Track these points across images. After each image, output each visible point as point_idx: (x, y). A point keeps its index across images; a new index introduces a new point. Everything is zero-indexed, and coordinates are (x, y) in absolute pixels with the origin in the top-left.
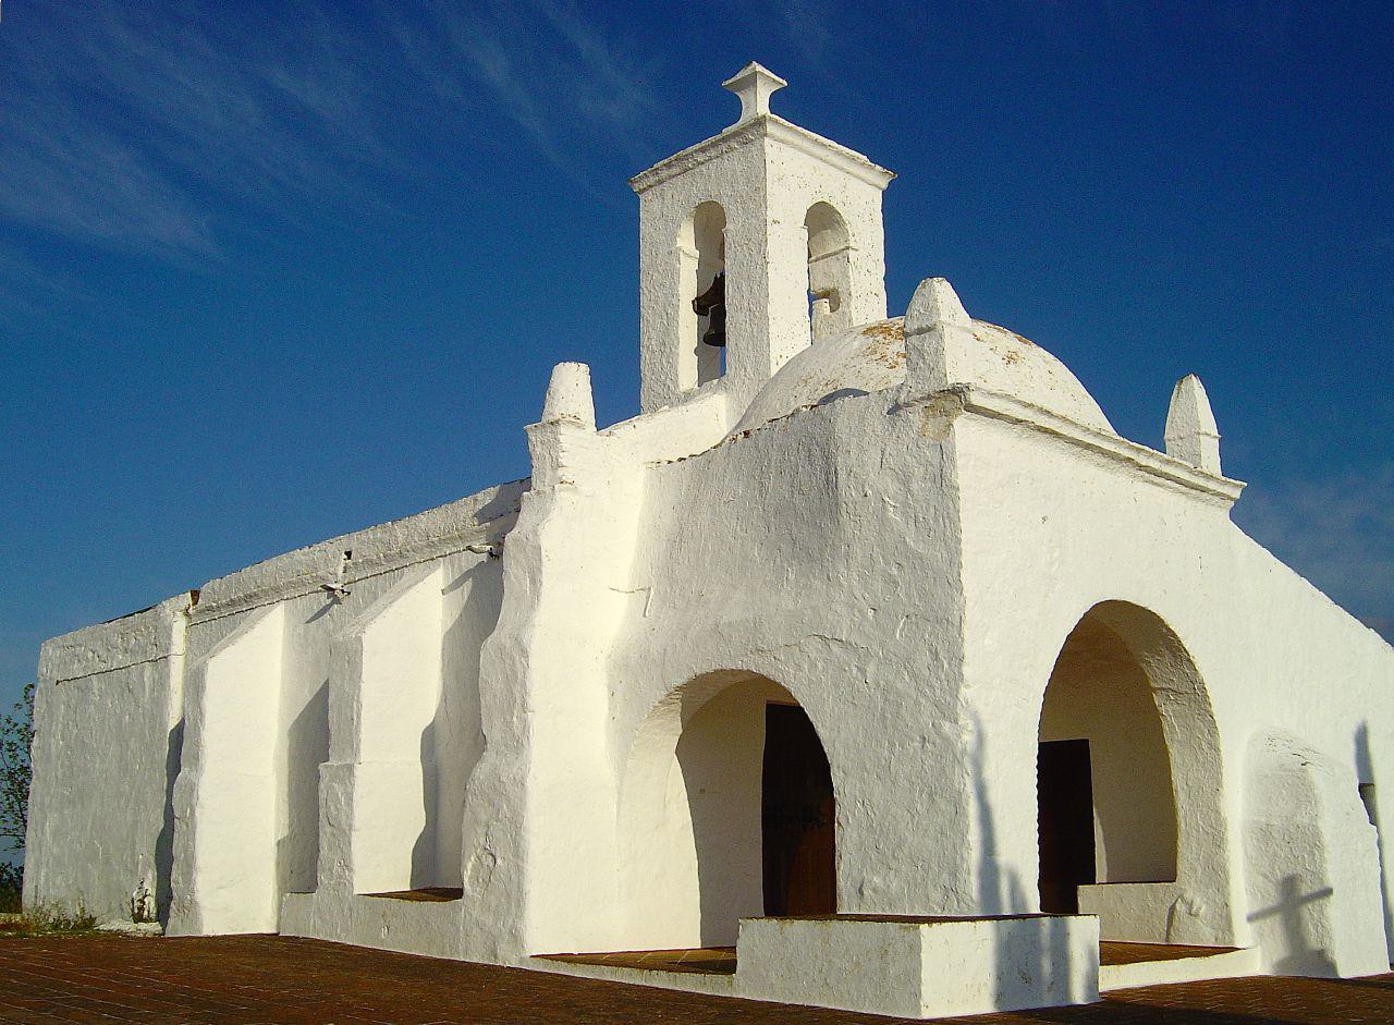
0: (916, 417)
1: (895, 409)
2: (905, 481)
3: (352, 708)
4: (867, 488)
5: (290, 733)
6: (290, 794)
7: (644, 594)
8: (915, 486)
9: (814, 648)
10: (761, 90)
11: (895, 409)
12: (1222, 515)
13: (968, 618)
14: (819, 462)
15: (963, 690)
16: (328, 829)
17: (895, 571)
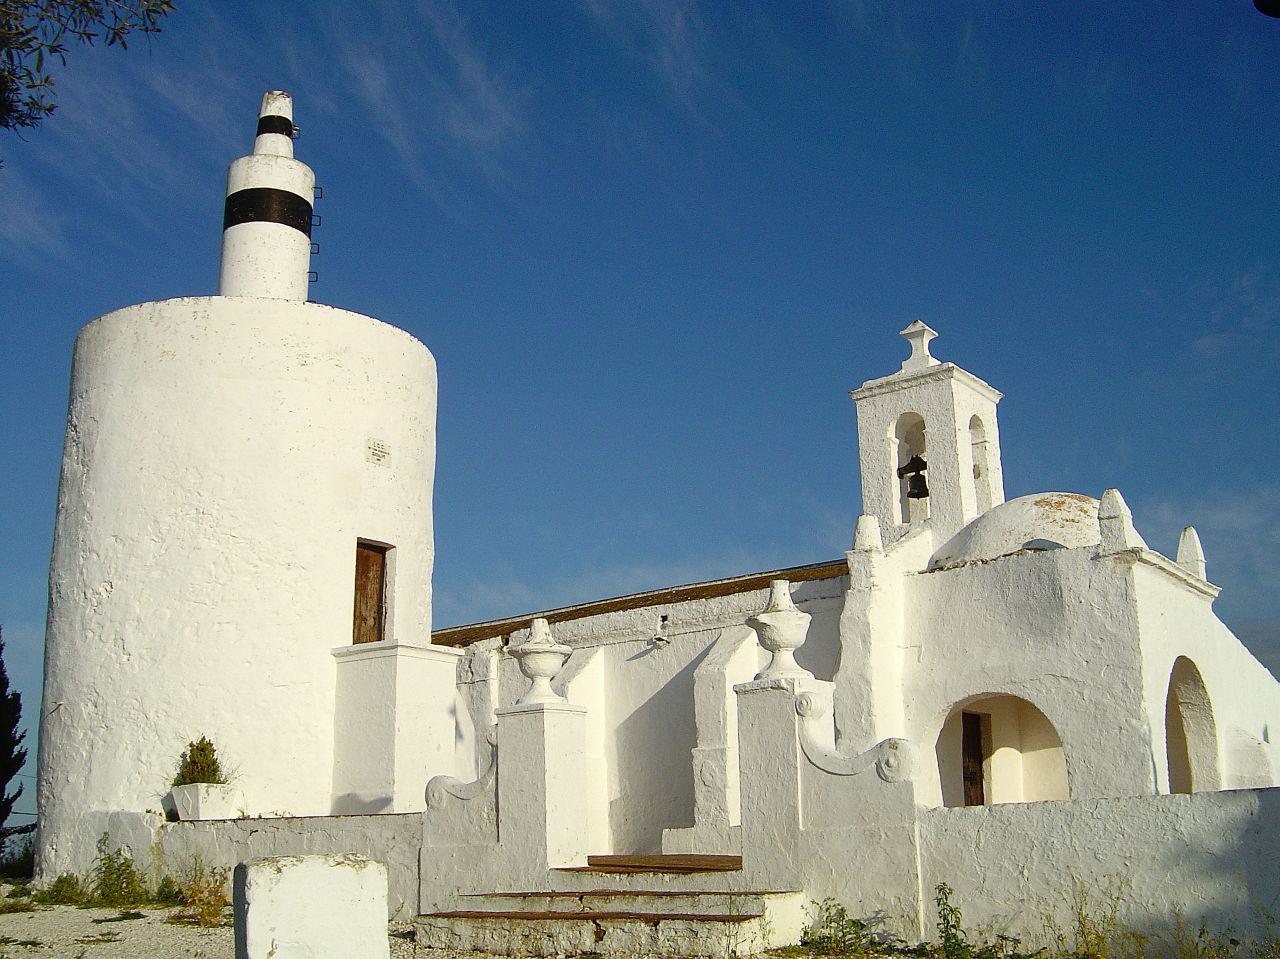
0: (1109, 563)
1: (1096, 557)
2: (1105, 597)
3: (718, 715)
4: (1081, 598)
5: (618, 731)
6: (621, 770)
7: (916, 649)
8: (1110, 598)
9: (1049, 682)
10: (922, 339)
11: (1096, 557)
12: (1206, 605)
13: (1144, 666)
14: (1046, 582)
15: (1143, 703)
16: (704, 788)
17: (1099, 642)
